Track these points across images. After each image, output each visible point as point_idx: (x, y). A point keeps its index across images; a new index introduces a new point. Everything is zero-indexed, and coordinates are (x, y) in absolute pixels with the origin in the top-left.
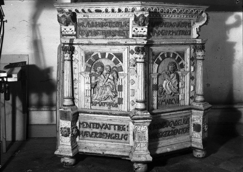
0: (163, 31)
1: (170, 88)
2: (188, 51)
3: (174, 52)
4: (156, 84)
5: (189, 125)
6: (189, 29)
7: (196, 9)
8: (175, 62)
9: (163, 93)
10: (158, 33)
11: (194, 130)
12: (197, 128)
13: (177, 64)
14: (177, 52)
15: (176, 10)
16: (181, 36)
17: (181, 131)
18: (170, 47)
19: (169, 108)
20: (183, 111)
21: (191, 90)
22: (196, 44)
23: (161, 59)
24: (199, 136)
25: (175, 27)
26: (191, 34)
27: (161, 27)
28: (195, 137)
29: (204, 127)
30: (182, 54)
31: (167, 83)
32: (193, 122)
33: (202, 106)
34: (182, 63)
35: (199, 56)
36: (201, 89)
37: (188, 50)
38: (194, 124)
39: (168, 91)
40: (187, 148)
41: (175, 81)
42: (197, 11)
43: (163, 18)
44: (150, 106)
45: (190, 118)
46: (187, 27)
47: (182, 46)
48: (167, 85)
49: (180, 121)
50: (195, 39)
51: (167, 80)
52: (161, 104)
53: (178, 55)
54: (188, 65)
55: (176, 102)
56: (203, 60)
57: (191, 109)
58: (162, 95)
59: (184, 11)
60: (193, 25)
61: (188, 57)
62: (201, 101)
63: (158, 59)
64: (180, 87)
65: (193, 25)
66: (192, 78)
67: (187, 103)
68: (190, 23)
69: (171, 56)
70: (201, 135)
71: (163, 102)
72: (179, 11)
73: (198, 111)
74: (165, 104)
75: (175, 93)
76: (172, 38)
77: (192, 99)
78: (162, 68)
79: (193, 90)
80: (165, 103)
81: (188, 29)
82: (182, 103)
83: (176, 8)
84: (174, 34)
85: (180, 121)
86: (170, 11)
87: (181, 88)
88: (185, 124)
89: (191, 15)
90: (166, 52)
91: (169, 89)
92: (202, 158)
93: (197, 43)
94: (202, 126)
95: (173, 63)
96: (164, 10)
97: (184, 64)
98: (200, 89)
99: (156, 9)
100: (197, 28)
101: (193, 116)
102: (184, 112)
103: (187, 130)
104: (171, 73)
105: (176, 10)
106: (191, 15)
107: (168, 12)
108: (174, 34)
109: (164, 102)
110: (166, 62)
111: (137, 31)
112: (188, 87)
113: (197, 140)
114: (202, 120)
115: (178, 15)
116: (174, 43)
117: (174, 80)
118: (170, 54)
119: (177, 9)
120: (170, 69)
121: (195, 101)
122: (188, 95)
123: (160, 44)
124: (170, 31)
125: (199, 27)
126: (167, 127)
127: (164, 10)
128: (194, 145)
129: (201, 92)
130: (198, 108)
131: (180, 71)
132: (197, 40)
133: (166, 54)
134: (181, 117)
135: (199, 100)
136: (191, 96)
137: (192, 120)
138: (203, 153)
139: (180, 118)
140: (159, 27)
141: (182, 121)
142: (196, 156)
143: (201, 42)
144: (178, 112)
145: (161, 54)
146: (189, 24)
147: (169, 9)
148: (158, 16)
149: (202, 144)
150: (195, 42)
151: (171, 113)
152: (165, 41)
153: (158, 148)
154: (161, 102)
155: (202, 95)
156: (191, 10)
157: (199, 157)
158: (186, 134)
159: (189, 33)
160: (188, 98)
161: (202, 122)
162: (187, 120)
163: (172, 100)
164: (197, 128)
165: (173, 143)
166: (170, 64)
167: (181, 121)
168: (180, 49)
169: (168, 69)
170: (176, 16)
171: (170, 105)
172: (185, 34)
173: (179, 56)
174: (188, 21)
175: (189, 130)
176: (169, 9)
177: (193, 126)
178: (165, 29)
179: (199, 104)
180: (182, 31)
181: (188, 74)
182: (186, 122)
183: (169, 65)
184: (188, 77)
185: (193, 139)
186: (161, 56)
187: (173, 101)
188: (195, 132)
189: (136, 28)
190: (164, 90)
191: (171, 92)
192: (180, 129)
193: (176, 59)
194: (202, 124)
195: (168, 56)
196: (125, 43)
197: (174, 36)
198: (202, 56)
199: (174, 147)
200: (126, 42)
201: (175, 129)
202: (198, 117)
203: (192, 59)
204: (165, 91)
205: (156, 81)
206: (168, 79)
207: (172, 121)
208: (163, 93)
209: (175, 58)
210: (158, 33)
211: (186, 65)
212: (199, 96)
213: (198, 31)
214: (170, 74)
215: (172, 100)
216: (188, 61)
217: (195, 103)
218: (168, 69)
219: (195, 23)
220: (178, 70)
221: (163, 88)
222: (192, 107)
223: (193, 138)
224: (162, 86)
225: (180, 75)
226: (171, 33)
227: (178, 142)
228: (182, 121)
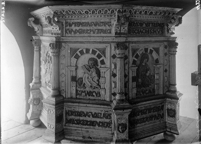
4: (75, 75)
6: (109, 28)
7: (105, 9)
20: (104, 105)
23: (79, 54)
25: (93, 26)
27: (78, 26)
58: (82, 87)
63: (137, 53)
74: (85, 95)
80: (85, 93)
82: (156, 93)
84: (92, 32)
103: (162, 116)
108: (92, 32)
117: (94, 74)
124: (88, 30)
126: (85, 116)
129: (119, 91)
136: (112, 92)
139: (100, 112)
146: (108, 22)
166: (91, 59)
173: (99, 53)
178: (83, 29)
205: (75, 73)
207: (91, 113)
226: (89, 31)
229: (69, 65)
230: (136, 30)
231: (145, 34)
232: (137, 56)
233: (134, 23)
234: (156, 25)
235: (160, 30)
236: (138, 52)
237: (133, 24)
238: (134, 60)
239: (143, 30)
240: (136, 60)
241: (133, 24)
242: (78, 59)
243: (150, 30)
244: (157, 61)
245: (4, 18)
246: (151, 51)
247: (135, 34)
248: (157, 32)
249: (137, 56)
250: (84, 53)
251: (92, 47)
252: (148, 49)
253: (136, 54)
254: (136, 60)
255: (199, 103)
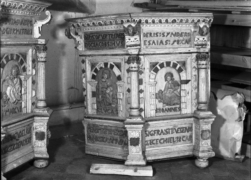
0: (7, 28)
1: (14, 95)
2: (30, 52)
3: (17, 54)
5: (31, 134)
8: (18, 65)
9: (7, 102)
10: (3, 31)
11: (36, 139)
12: (40, 136)
13: (19, 67)
14: (20, 54)
15: (23, 5)
16: (24, 35)
17: (24, 142)
18: (15, 48)
19: (14, 118)
21: (33, 96)
22: (38, 44)
23: (159, 68)
24: (43, 144)
26: (33, 33)
28: (38, 147)
29: (48, 135)
30: (25, 56)
31: (11, 90)
32: (35, 131)
33: (47, 112)
34: (25, 66)
35: (42, 58)
36: (44, 93)
37: (30, 50)
38: (37, 133)
39: (12, 98)
40: (31, 159)
41: (18, 86)
42: (40, 8)
43: (11, 13)
44: (189, 115)
45: (32, 126)
46: (29, 25)
47: (25, 46)
48: (11, 92)
49: (24, 132)
50: (37, 40)
51: (11, 86)
52: (5, 114)
53: (21, 58)
54: (31, 68)
55: (18, 111)
56: (45, 62)
57: (33, 116)
59: (29, 7)
60: (35, 23)
61: (31, 59)
62: (44, 107)
64: (23, 93)
65: (35, 23)
66: (34, 82)
67: (30, 111)
68: (31, 21)
69: (15, 59)
70: (46, 143)
71: (7, 112)
72: (25, 7)
73: (42, 118)
75: (18, 101)
76: (16, 37)
77: (33, 106)
78: (6, 72)
79: (35, 96)
81: (30, 28)
82: (24, 111)
83: (37, 5)
85: (24, 132)
86: (16, 6)
87: (23, 94)
88: (28, 134)
89: (33, 12)
90: (10, 54)
91: (13, 96)
92: (46, 167)
93: (39, 43)
94: (46, 133)
95: (16, 66)
96: (11, 4)
97: (26, 67)
98: (42, 94)
99: (4, 3)
100: (39, 27)
101: (35, 124)
102: (28, 120)
103: (29, 140)
104: (15, 78)
105: (23, 5)
106: (33, 12)
107: (14, 8)
109: (8, 112)
110: (9, 66)
111: (199, 40)
112: (30, 92)
113: (40, 149)
114: (46, 126)
115: (22, 11)
116: (19, 43)
117: (17, 86)
118: (14, 56)
119: (23, 3)
120: (13, 73)
121: (37, 107)
122: (30, 101)
123: (6, 44)
124: (14, 30)
125: (41, 26)
127: (11, 4)
128: (37, 155)
129: (44, 97)
130: (43, 114)
131: (22, 75)
132: (39, 40)
133: (10, 56)
134: (24, 127)
135: (41, 105)
137: (34, 128)
138: (46, 162)
139: (24, 128)
140: (4, 25)
141: (25, 131)
142: (39, 167)
143: (44, 43)
144: (23, 122)
145: (5, 56)
147: (16, 4)
148: (7, 11)
149: (47, 153)
150: (37, 43)
151: (17, 124)
152: (11, 41)
153: (7, 165)
154: (5, 112)
155: (44, 100)
156: (35, 6)
157: (42, 167)
158: (28, 144)
159: (30, 32)
160: (30, 104)
161: (46, 128)
162: (29, 130)
163: (15, 108)
164: (40, 136)
165: (18, 157)
167: (25, 132)
168: (23, 49)
169: (11, 74)
170: (21, 12)
171: (14, 115)
172: (28, 34)
174: (29, 18)
175: (31, 139)
176: (16, 4)
177: (35, 135)
179: (42, 109)
180: (25, 30)
181: (31, 78)
182: (29, 131)
183: (12, 68)
184: (30, 81)
185: (35, 149)
186: (5, 58)
187: (16, 110)
188: (38, 140)
189: (198, 38)
190: (8, 98)
191: (15, 100)
192: (24, 141)
193: (19, 61)
194: (46, 131)
195: (12, 59)
196: (188, 51)
197: (18, 35)
198: (45, 58)
199: (20, 162)
200: (189, 51)
201: (19, 141)
202: (42, 124)
203: (33, 61)
204: (9, 99)
206: (11, 85)
208: (7, 102)
209: (18, 61)
210: (3, 31)
211: (28, 68)
212: (42, 102)
213: (40, 30)
214: (13, 79)
215: (15, 108)
216: (30, 63)
217: (38, 110)
218: (11, 74)
219: (37, 21)
220: (20, 74)
221: (7, 96)
222: (35, 114)
223: (36, 148)
224: (6, 94)
225: (23, 79)
226: (15, 32)
227: (22, 155)
228: (25, 131)
229: (154, 80)
230: (92, 43)
231: (102, 47)
232: (96, 71)
233: (90, 36)
234: (114, 36)
235: (119, 42)
236: (97, 67)
237: (88, 37)
238: (93, 74)
239: (99, 43)
240: (95, 74)
241: (88, 37)
242: (156, 72)
243: (107, 42)
244: (119, 78)
245: (209, 27)
246: (112, 67)
247: (91, 47)
248: (116, 44)
249: (96, 71)
250: (164, 66)
251: (173, 59)
252: (170, 62)
253: (94, 69)
254: (95, 74)
255: (226, 150)
